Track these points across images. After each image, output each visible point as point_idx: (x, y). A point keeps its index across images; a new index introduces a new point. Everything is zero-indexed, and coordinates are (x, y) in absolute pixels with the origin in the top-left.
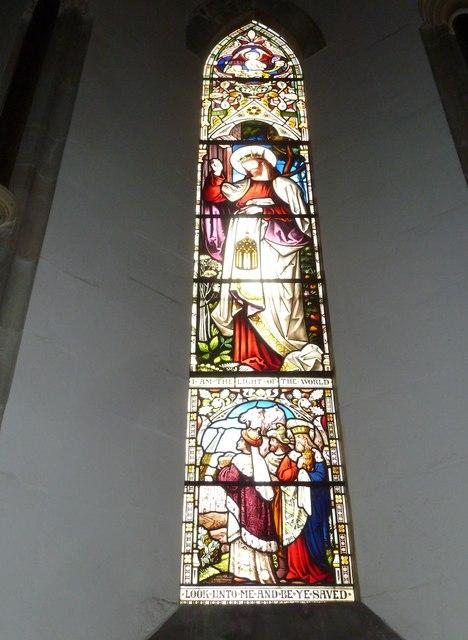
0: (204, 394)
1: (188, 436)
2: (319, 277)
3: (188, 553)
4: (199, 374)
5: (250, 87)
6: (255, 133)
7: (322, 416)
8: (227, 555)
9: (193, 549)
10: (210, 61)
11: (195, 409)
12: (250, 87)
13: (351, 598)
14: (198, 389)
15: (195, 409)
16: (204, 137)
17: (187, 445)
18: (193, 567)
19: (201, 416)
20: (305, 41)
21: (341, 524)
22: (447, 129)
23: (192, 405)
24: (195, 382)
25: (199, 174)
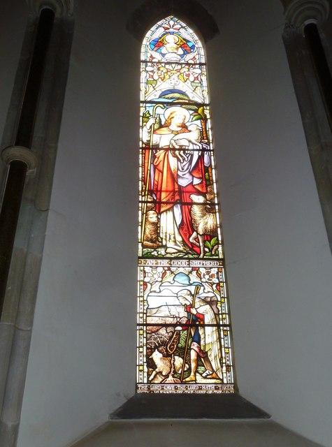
0: (147, 269)
3: (141, 365)
5: (172, 67)
6: (173, 99)
12: (172, 67)
13: (232, 391)
20: (207, 31)
23: (140, 276)
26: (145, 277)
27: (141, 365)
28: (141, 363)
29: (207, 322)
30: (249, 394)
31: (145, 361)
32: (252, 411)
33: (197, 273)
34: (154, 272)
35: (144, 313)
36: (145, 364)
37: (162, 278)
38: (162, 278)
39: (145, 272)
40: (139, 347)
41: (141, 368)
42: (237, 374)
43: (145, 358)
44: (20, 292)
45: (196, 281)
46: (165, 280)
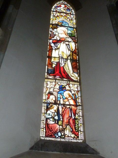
0: (48, 83)
1: (43, 105)
2: (78, 59)
3: (43, 128)
4: (47, 78)
5: (63, 22)
7: (77, 91)
8: (64, 61)
9: (44, 128)
10: (53, 7)
11: (46, 86)
12: (63, 22)
14: (47, 82)
15: (46, 86)
16: (51, 23)
17: (42, 115)
18: (43, 132)
19: (48, 88)
21: (80, 109)
22: (108, 13)
23: (45, 85)
24: (46, 80)
25: (47, 62)
26: (47, 85)
27: (43, 128)
28: (43, 127)
29: (69, 60)
30: (92, 145)
31: (44, 127)
32: (94, 152)
33: (69, 86)
34: (51, 84)
35: (45, 113)
36: (45, 128)
37: (54, 86)
38: (54, 86)
39: (47, 84)
40: (42, 121)
41: (43, 122)
42: (86, 137)
43: (45, 125)
44: (17, 15)
45: (68, 89)
46: (55, 87)
